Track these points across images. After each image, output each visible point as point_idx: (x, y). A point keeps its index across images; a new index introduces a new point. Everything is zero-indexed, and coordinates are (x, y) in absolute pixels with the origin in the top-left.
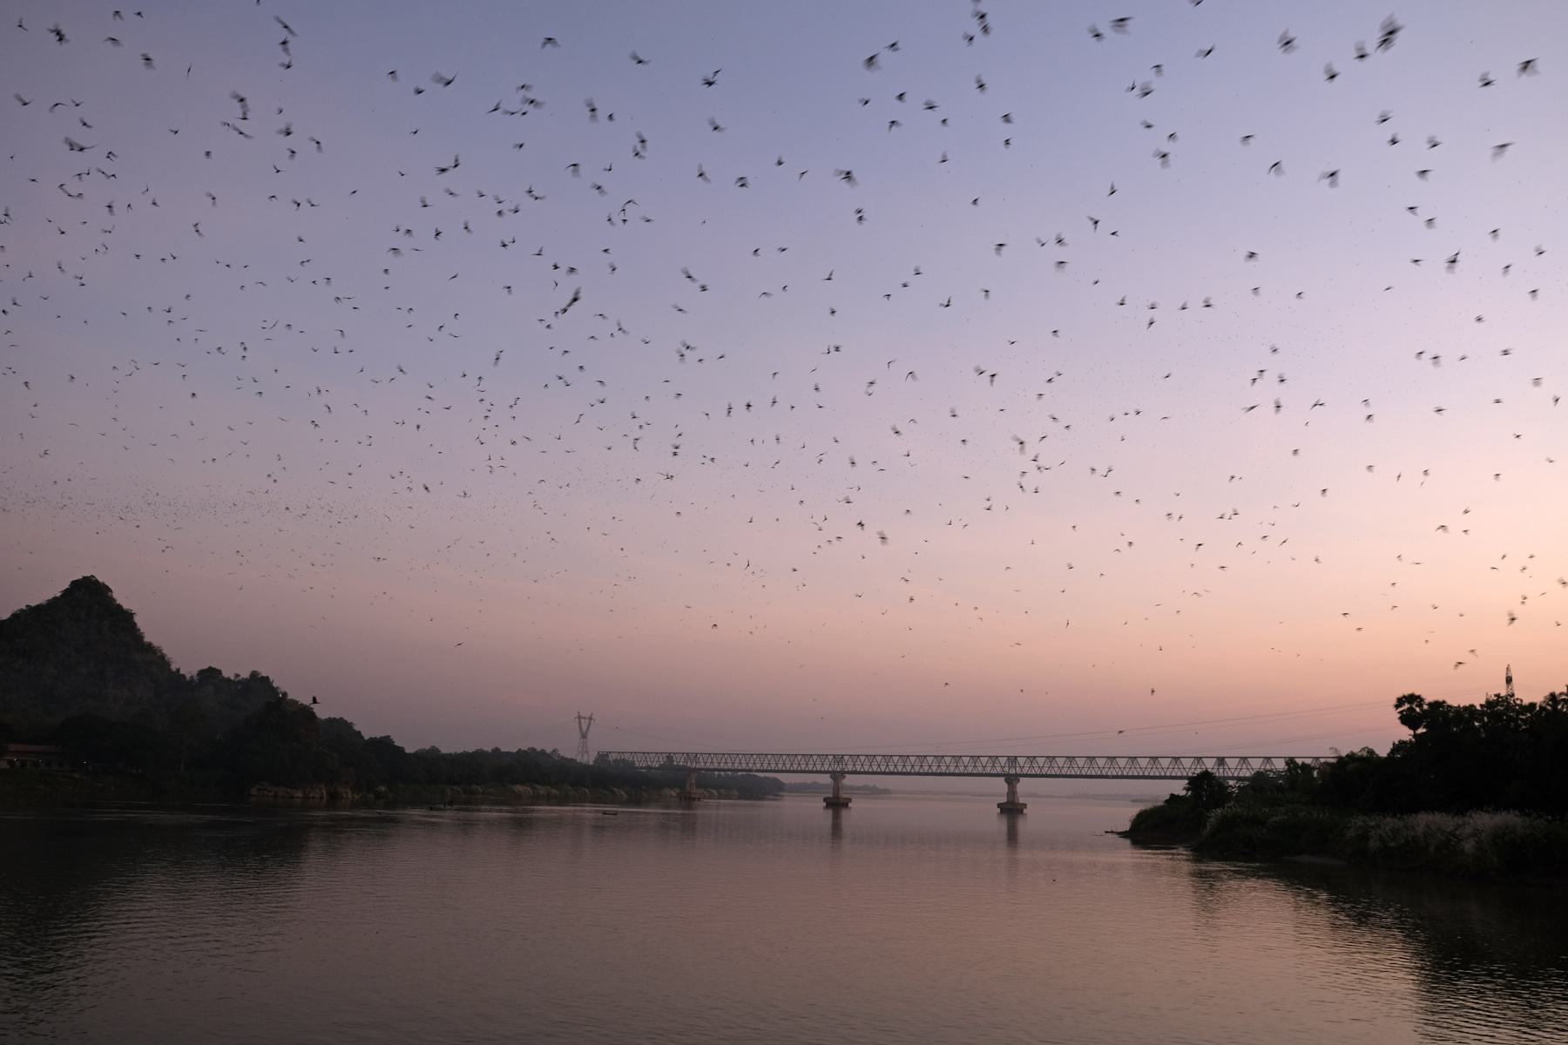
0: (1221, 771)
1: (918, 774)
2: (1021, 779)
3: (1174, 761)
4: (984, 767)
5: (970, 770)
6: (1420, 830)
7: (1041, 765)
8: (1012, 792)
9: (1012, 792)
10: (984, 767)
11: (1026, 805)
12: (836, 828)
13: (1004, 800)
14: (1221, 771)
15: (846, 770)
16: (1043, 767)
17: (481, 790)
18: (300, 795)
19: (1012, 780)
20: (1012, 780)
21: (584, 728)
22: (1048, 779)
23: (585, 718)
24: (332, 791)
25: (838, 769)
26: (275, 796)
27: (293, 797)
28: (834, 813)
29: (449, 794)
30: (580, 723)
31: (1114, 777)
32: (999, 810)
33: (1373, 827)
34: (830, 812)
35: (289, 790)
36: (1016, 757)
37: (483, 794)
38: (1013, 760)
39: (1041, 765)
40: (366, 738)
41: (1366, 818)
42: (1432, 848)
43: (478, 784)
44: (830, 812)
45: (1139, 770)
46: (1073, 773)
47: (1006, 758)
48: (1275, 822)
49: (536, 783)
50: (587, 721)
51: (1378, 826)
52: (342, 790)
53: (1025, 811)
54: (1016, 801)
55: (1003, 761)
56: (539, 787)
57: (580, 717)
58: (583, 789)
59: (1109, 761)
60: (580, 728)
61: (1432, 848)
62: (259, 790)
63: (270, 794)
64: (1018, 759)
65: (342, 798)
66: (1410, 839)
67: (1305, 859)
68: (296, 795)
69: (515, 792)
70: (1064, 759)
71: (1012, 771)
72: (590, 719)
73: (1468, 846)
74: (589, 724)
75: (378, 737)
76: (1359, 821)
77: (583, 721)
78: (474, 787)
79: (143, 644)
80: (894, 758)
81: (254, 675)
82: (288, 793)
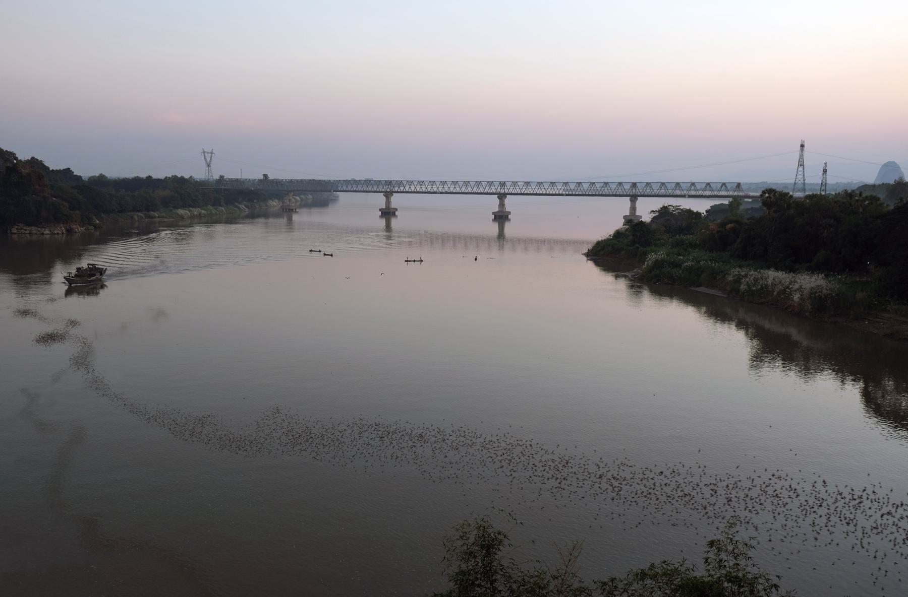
0: (634, 191)
1: (441, 193)
2: (508, 196)
4: (461, 188)
6: (770, 281)
10: (461, 188)
12: (388, 228)
13: (497, 210)
14: (634, 191)
15: (394, 190)
17: (157, 215)
18: (47, 232)
19: (502, 196)
20: (502, 196)
21: (208, 160)
23: (208, 153)
24: (68, 228)
25: (388, 190)
26: (30, 234)
27: (43, 234)
29: (137, 219)
30: (205, 156)
31: (567, 195)
33: (743, 276)
35: (39, 229)
36: (505, 182)
37: (159, 217)
40: (51, 169)
41: (740, 270)
42: (775, 293)
43: (153, 211)
45: (543, 190)
46: (529, 192)
48: (687, 265)
49: (191, 207)
50: (210, 155)
51: (746, 276)
53: (510, 217)
54: (504, 210)
55: (497, 185)
57: (204, 152)
58: (221, 208)
59: (564, 185)
60: (205, 159)
61: (775, 293)
62: (17, 229)
63: (26, 232)
64: (637, 184)
65: (76, 232)
66: (764, 286)
67: (702, 289)
68: (45, 232)
69: (178, 214)
71: (502, 191)
72: (212, 153)
73: (796, 297)
74: (211, 157)
75: (62, 169)
76: (736, 271)
77: (206, 154)
78: (152, 213)
82: (39, 231)
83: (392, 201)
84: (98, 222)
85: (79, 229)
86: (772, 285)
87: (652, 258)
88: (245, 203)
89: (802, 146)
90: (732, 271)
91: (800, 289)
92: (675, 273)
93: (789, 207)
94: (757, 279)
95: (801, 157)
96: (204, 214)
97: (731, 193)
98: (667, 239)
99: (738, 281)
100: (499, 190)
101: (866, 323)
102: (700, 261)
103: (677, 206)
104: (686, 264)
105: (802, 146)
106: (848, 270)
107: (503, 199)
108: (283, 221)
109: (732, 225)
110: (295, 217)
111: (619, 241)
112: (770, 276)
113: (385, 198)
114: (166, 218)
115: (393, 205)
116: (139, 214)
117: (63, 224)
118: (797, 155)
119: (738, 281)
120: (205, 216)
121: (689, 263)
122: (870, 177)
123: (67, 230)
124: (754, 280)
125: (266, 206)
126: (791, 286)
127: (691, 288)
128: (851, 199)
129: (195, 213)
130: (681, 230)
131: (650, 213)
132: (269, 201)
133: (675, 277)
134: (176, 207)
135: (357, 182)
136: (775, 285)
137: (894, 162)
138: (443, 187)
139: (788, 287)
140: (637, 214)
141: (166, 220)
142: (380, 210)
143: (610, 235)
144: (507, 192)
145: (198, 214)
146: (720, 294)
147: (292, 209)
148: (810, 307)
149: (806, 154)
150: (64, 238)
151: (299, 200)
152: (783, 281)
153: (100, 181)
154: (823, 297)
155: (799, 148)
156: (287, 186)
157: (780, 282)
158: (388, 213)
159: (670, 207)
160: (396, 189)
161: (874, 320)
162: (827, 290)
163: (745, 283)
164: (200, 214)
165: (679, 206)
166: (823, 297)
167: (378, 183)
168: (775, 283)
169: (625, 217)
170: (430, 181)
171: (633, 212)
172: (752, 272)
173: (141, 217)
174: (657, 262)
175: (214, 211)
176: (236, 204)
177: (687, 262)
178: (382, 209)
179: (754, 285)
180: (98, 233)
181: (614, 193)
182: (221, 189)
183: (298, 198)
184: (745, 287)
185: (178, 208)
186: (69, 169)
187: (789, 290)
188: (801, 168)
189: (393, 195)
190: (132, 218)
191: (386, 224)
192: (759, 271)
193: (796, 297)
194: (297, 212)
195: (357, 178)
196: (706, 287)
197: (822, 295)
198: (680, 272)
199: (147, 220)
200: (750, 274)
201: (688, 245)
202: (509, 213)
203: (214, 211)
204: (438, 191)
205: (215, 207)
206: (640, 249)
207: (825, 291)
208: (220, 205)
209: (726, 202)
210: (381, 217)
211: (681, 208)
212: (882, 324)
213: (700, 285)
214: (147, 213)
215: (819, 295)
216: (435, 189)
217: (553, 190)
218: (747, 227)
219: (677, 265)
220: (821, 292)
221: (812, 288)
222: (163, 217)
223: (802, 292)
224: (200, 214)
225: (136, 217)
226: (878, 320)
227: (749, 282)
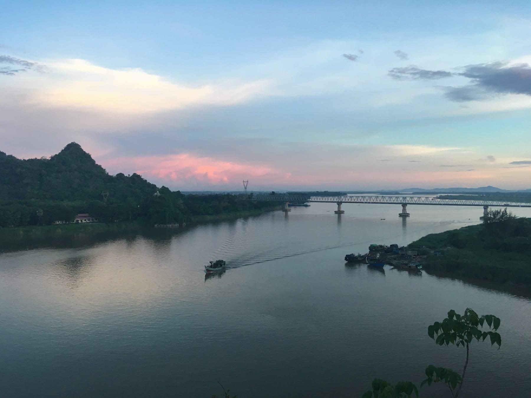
0: (486, 203)
2: (408, 205)
3: (426, 199)
4: (367, 200)
8: (404, 209)
9: (404, 209)
10: (367, 200)
11: (344, 211)
15: (342, 201)
16: (409, 201)
19: (404, 205)
20: (404, 205)
21: (246, 185)
22: (389, 204)
25: (339, 201)
28: (338, 216)
30: (244, 183)
34: (337, 215)
39: (394, 200)
45: (429, 202)
47: (402, 198)
50: (246, 183)
57: (244, 182)
60: (244, 185)
62: (157, 225)
64: (407, 198)
70: (417, 198)
71: (404, 202)
72: (247, 182)
74: (247, 183)
77: (245, 183)
79: (115, 178)
80: (373, 197)
81: (135, 174)
100: (402, 201)
107: (405, 206)
115: (342, 209)
135: (364, 192)
138: (370, 200)
144: (407, 203)
160: (344, 201)
167: (379, 192)
181: (473, 204)
189: (407, 206)
204: (364, 202)
217: (443, 202)
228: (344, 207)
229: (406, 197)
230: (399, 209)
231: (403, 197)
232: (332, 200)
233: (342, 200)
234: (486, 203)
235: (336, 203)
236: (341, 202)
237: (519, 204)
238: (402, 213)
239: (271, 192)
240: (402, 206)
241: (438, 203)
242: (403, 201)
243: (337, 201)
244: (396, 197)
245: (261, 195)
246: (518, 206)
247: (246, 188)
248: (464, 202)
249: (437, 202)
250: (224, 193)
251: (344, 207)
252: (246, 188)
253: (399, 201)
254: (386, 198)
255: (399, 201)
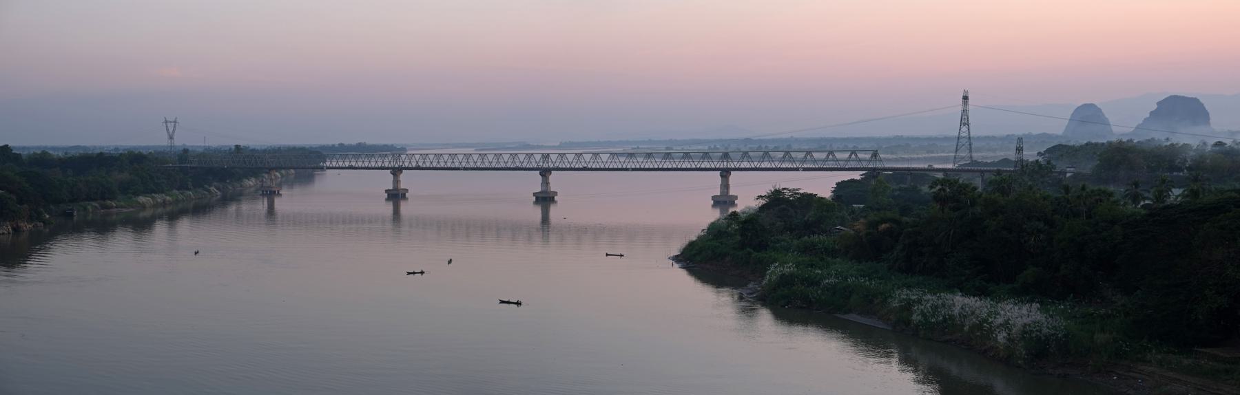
1: (465, 169)
2: (552, 172)
5: (435, 165)
6: (956, 311)
7: (506, 161)
8: (725, 186)
9: (725, 186)
11: (557, 193)
13: (538, 189)
15: (404, 166)
19: (545, 173)
20: (545, 173)
21: (171, 130)
25: (397, 166)
29: (91, 210)
31: (633, 170)
32: (534, 198)
33: (914, 301)
37: (116, 207)
38: (546, 157)
42: (966, 328)
44: (391, 204)
48: (827, 283)
50: (173, 124)
51: (919, 301)
52: (22, 224)
53: (556, 198)
54: (549, 190)
56: (156, 196)
57: (166, 122)
60: (168, 130)
61: (966, 328)
64: (730, 154)
67: (853, 317)
69: (139, 203)
71: (545, 166)
72: (175, 122)
73: (1001, 337)
74: (175, 127)
76: (904, 294)
77: (169, 124)
83: (401, 179)
84: (47, 216)
85: (27, 226)
86: (960, 315)
87: (775, 271)
88: (215, 183)
89: (966, 98)
90: (897, 293)
91: (1006, 325)
92: (812, 294)
93: (973, 204)
94: (937, 307)
95: (965, 112)
96: (169, 201)
97: (865, 165)
98: (790, 241)
99: (908, 306)
100: (541, 164)
101: (1115, 378)
102: (846, 278)
103: (794, 189)
104: (827, 281)
105: (966, 98)
106: (1072, 295)
108: (262, 206)
109: (887, 225)
110: (279, 204)
111: (722, 243)
112: (956, 304)
113: (392, 176)
114: (125, 208)
115: (402, 186)
116: (94, 204)
117: (9, 221)
118: (960, 108)
119: (908, 306)
120: (170, 203)
121: (832, 281)
122: (1056, 127)
123: (14, 229)
124: (932, 309)
125: (241, 186)
126: (990, 320)
127: (836, 315)
128: (1067, 193)
129: (159, 200)
130: (808, 228)
131: (757, 199)
132: (244, 180)
133: (813, 300)
134: (136, 194)
136: (965, 316)
137: (1091, 106)
139: (985, 321)
140: (731, 193)
141: (125, 210)
142: (386, 191)
143: (703, 230)
145: (162, 201)
146: (880, 325)
147: (275, 192)
148: (1024, 352)
149: (970, 108)
150: (10, 237)
151: (280, 176)
152: (978, 312)
153: (42, 160)
154: (1043, 338)
155: (961, 101)
156: (268, 163)
157: (973, 313)
158: (396, 196)
159: (785, 191)
160: (406, 164)
161: (1126, 374)
162: (1048, 328)
163: (919, 312)
164: (164, 201)
165: (797, 190)
166: (1043, 338)
168: (965, 314)
169: (714, 198)
170: (450, 154)
171: (726, 191)
172: (929, 297)
173: (96, 207)
174: (783, 276)
175: (181, 197)
176: (206, 186)
177: (829, 279)
178: (389, 190)
179: (933, 316)
180: (47, 230)
182: (187, 167)
183: (277, 174)
184: (920, 318)
185: (138, 195)
186: (7, 146)
187: (988, 326)
188: (964, 129)
190: (85, 209)
191: (394, 211)
192: (938, 295)
193: (1001, 337)
194: (281, 195)
195: (347, 142)
196: (858, 314)
197: (1041, 335)
198: (819, 292)
199: (102, 211)
200: (925, 298)
201: (823, 250)
202: (556, 193)
203: (181, 197)
205: (181, 191)
206: (753, 255)
207: (1045, 330)
208: (188, 189)
209: (857, 176)
210: (388, 199)
211: (801, 192)
212: (1140, 381)
213: (850, 311)
214: (102, 202)
215: (1037, 336)
216: (457, 165)
218: (910, 229)
219: (814, 283)
220: (1040, 331)
221: (1025, 324)
222: (122, 207)
223: (1010, 330)
224: (164, 201)
225: (89, 207)
226: (1132, 374)
227: (925, 311)
228: (406, 179)
229: (548, 154)
230: (534, 182)
231: (543, 154)
232: (379, 164)
233: (403, 162)
234: (724, 165)
235: (389, 171)
236: (400, 169)
237: (906, 166)
238: (719, 194)
239: (233, 148)
240: (722, 176)
241: (620, 167)
242: (543, 162)
243: (390, 166)
244: (527, 154)
245: (208, 155)
246: (797, 169)
247: (171, 138)
248: (658, 163)
249: (618, 163)
250: (117, 149)
251: (406, 179)
252: (171, 138)
253: (487, 164)
254: (520, 156)
255: (487, 164)
